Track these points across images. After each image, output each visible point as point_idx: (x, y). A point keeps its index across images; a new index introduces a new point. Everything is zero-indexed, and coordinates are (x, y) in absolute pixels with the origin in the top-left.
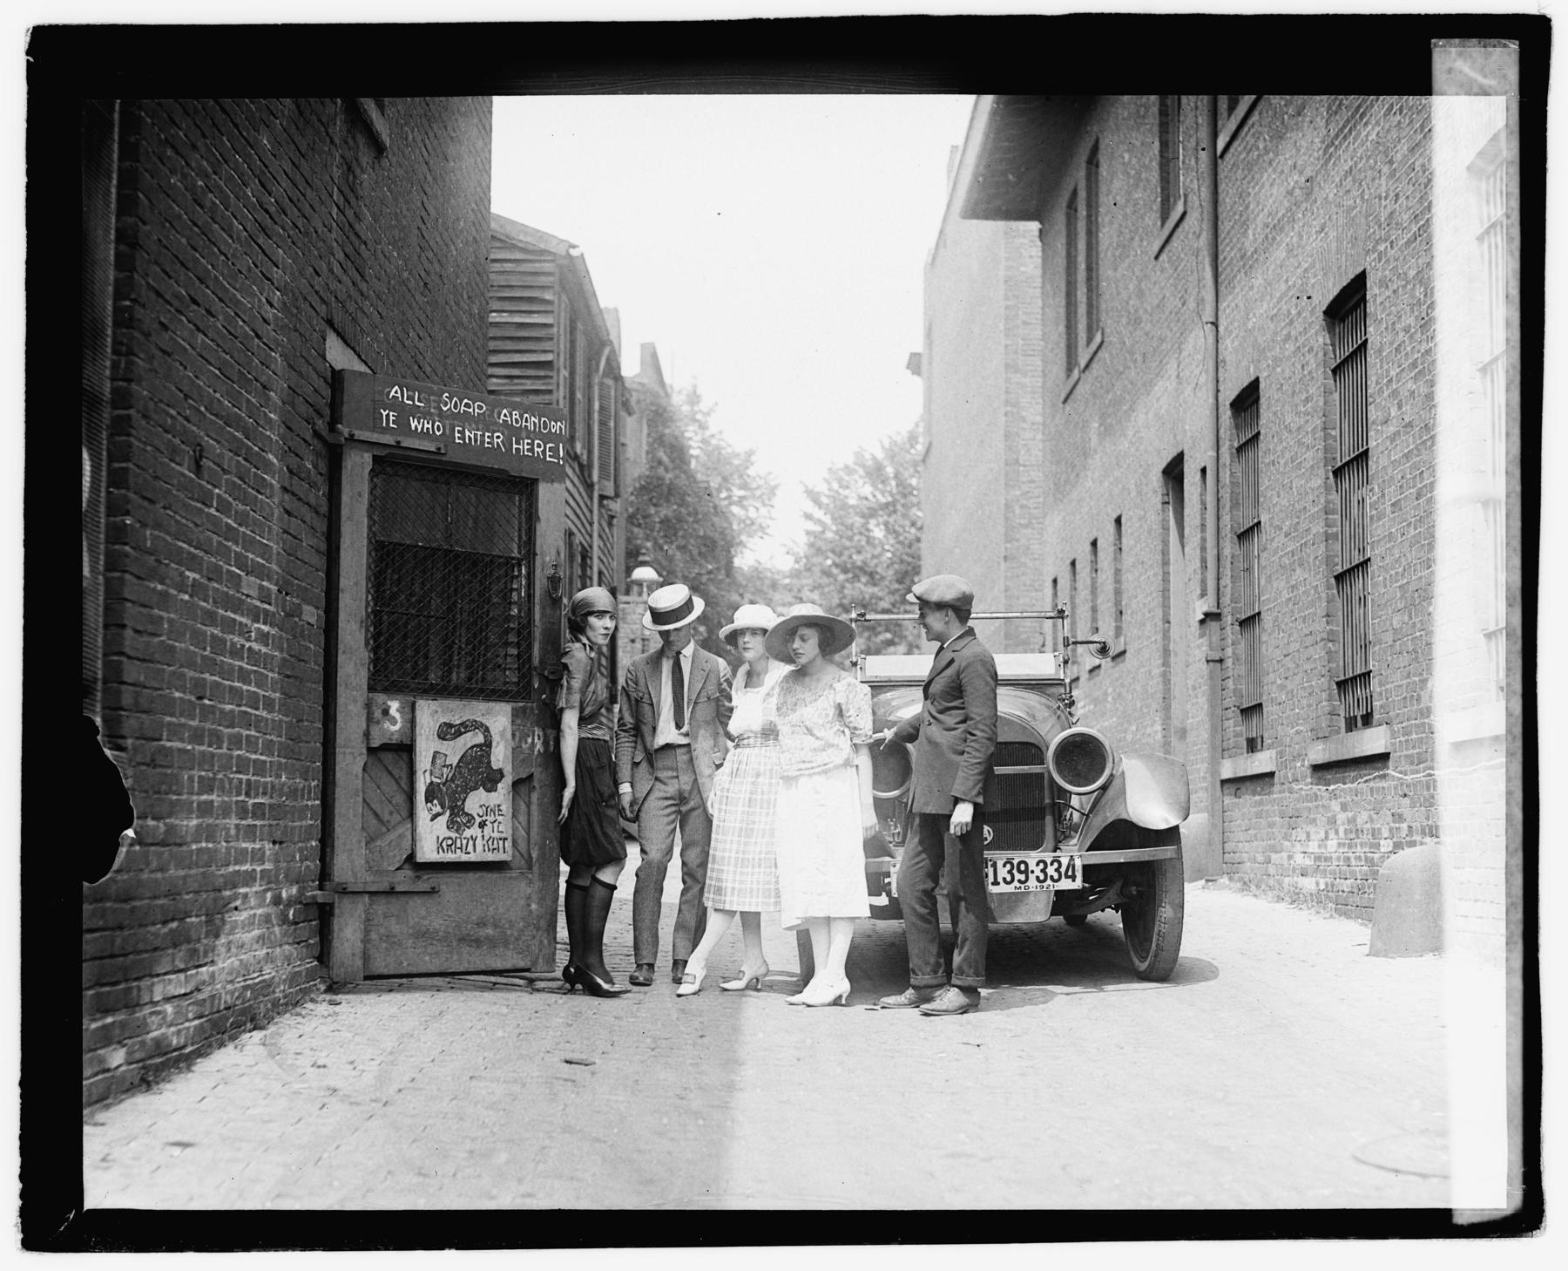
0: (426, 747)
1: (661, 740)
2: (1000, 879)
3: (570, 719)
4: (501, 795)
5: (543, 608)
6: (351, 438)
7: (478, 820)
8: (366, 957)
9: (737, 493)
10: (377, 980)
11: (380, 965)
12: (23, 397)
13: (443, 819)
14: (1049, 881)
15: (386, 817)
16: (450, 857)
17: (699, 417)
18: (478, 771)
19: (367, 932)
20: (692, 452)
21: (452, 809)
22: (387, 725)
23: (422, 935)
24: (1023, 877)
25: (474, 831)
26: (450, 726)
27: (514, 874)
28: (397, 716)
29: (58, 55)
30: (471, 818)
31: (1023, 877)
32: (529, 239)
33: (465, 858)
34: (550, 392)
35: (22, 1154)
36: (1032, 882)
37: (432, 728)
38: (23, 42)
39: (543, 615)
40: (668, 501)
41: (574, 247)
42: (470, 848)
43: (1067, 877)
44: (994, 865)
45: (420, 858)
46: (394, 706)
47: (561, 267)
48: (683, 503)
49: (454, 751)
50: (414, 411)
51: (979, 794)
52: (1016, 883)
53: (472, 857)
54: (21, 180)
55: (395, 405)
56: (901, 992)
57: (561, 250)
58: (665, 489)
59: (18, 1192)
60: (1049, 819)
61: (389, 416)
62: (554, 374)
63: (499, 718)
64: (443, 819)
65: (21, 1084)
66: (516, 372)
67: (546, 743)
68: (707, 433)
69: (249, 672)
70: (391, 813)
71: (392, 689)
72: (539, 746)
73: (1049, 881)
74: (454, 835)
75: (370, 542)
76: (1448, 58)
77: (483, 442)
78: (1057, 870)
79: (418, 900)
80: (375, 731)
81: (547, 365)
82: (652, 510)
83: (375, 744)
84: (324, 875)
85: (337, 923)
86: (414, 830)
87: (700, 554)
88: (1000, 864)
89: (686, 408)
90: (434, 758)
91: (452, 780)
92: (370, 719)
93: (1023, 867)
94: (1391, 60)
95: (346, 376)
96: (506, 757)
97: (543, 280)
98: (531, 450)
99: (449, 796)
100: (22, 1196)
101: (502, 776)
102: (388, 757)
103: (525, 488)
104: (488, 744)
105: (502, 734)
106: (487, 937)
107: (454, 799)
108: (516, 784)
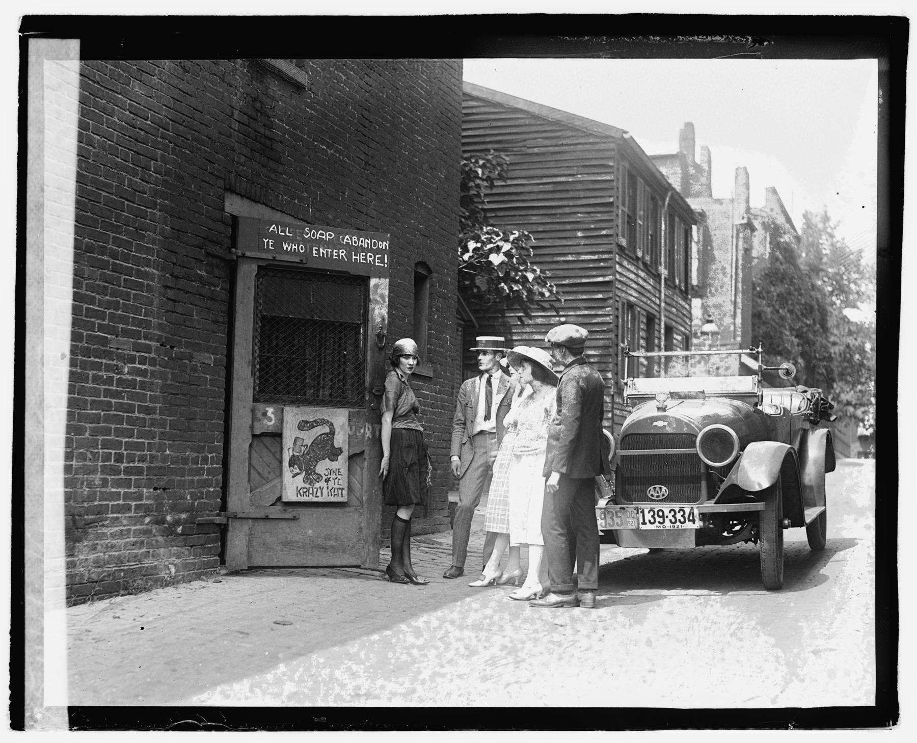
0: (290, 434)
1: (478, 429)
2: (647, 521)
3: (387, 418)
4: (341, 463)
5: (373, 353)
6: (243, 256)
7: (325, 477)
8: (249, 557)
9: (856, 276)
10: (253, 570)
11: (258, 561)
13: (300, 478)
14: (678, 523)
15: (266, 475)
16: (305, 499)
17: (829, 230)
18: (325, 448)
19: (250, 541)
20: (824, 252)
21: (307, 471)
22: (265, 421)
23: (287, 544)
24: (661, 520)
25: (322, 484)
26: (307, 422)
27: (352, 509)
28: (273, 416)
30: (320, 476)
31: (661, 520)
32: (600, 130)
33: (315, 500)
34: (612, 220)
36: (668, 524)
37: (294, 423)
38: (17, 24)
39: (372, 357)
40: (782, 282)
41: (626, 132)
42: (319, 494)
43: (689, 520)
44: (643, 512)
45: (284, 499)
46: (270, 411)
47: (619, 145)
48: (792, 283)
49: (309, 437)
50: (286, 239)
51: (563, 465)
52: (657, 524)
53: (320, 499)
55: (273, 236)
57: (618, 135)
58: (780, 276)
60: (704, 484)
61: (269, 243)
62: (614, 209)
63: (340, 418)
64: (300, 478)
65: (11, 633)
66: (589, 210)
67: (373, 433)
68: (835, 240)
69: (121, 392)
70: (269, 473)
71: (269, 401)
72: (369, 434)
73: (678, 523)
74: (308, 486)
75: (255, 314)
77: (332, 255)
78: (683, 516)
79: (283, 524)
80: (256, 424)
81: (611, 204)
82: (772, 289)
83: (257, 432)
84: (224, 507)
85: (230, 534)
86: (281, 482)
87: (802, 314)
88: (646, 511)
89: (820, 226)
90: (295, 441)
91: (308, 454)
92: (254, 419)
93: (661, 514)
95: (241, 220)
96: (344, 441)
97: (608, 154)
98: (366, 259)
99: (305, 463)
101: (342, 452)
102: (267, 440)
103: (362, 281)
104: (332, 433)
105: (342, 427)
106: (332, 547)
107: (308, 464)
108: (351, 458)
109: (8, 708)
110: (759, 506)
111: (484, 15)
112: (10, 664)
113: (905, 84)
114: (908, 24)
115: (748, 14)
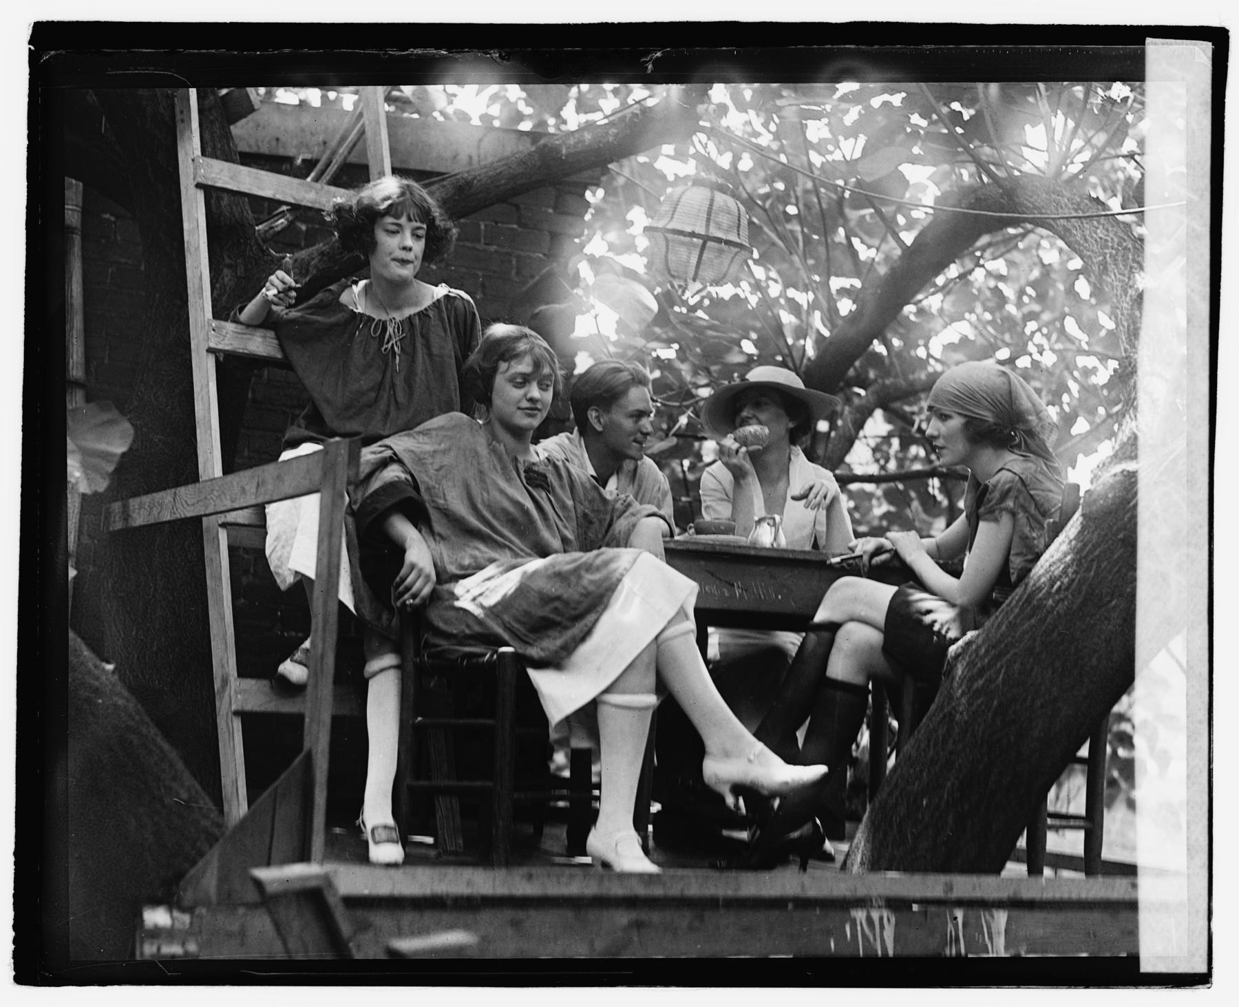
12: (23, 313)
29: (30, 969)
35: (15, 909)
38: (27, 33)
54: (24, 142)
56: (545, 146)
59: (11, 939)
65: (15, 854)
76: (1154, 48)
94: (1105, 54)
100: (15, 941)
109: (10, 955)
110: (869, 487)
111: (655, 23)
112: (14, 895)
113: (1223, 117)
114: (1228, 38)
115: (1012, 22)
